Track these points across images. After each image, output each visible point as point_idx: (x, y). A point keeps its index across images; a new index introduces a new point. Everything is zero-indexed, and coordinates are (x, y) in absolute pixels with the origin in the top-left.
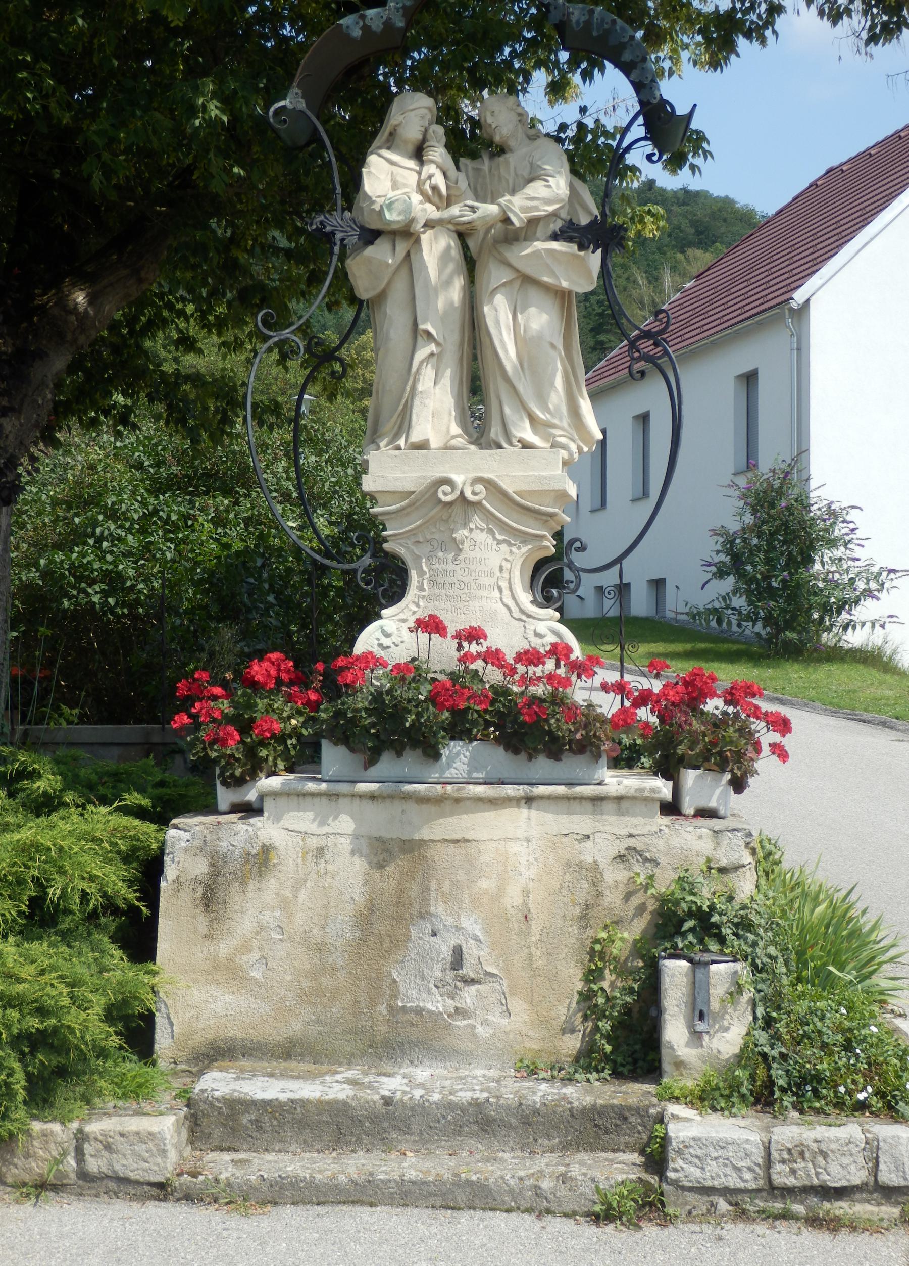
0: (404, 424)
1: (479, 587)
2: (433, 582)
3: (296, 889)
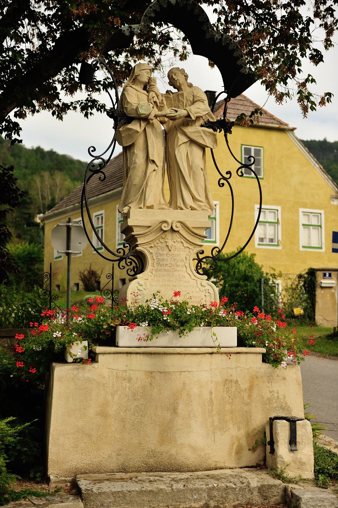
0: (143, 197)
1: (178, 266)
2: (158, 264)
3: (113, 395)
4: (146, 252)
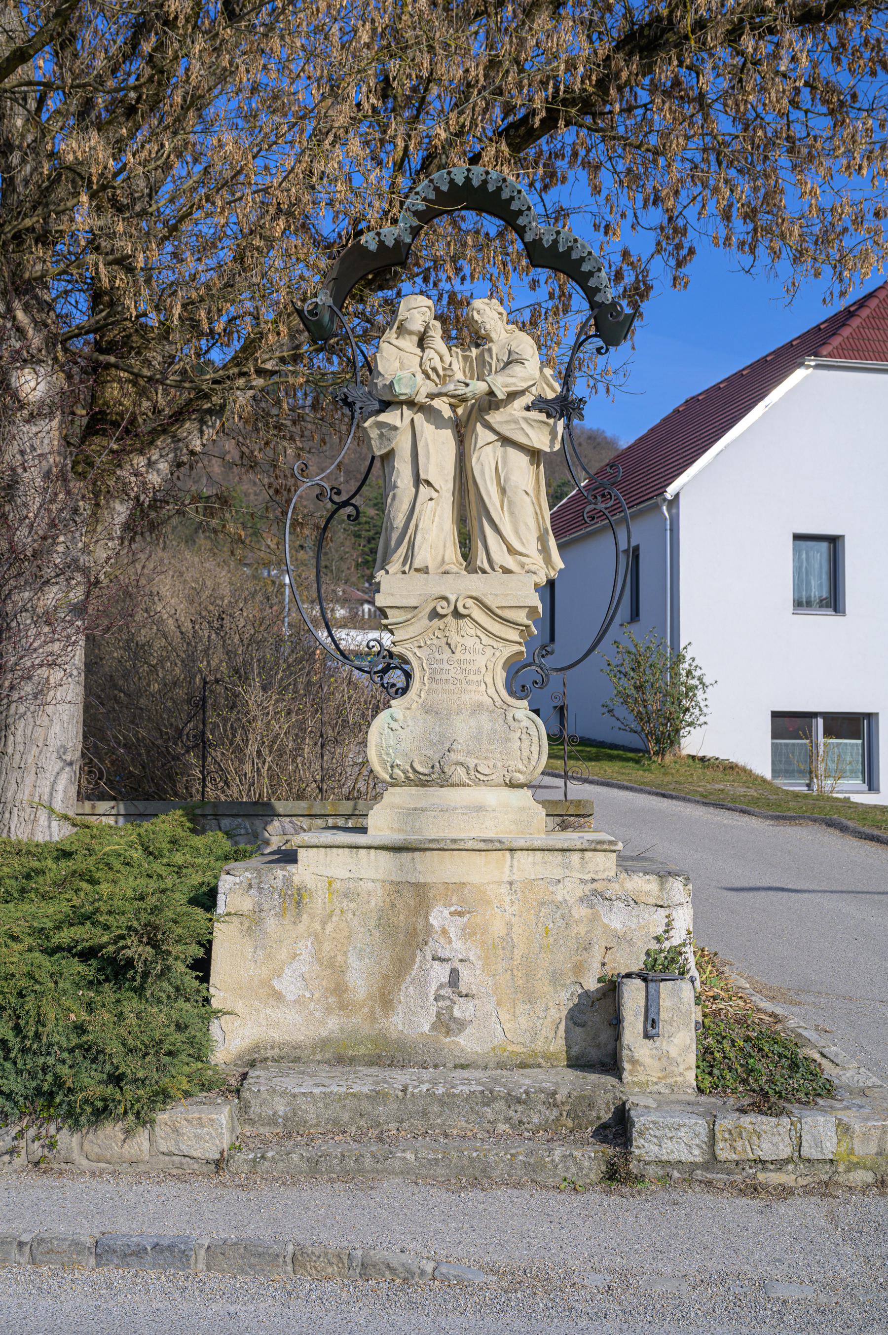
1: (469, 682)
3: (324, 924)
4: (410, 656)
